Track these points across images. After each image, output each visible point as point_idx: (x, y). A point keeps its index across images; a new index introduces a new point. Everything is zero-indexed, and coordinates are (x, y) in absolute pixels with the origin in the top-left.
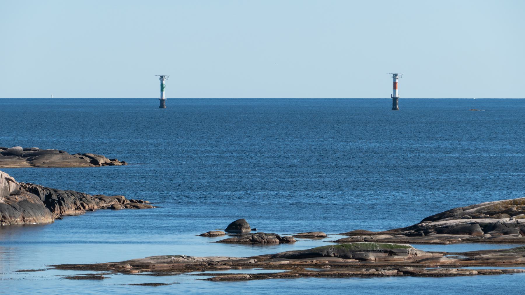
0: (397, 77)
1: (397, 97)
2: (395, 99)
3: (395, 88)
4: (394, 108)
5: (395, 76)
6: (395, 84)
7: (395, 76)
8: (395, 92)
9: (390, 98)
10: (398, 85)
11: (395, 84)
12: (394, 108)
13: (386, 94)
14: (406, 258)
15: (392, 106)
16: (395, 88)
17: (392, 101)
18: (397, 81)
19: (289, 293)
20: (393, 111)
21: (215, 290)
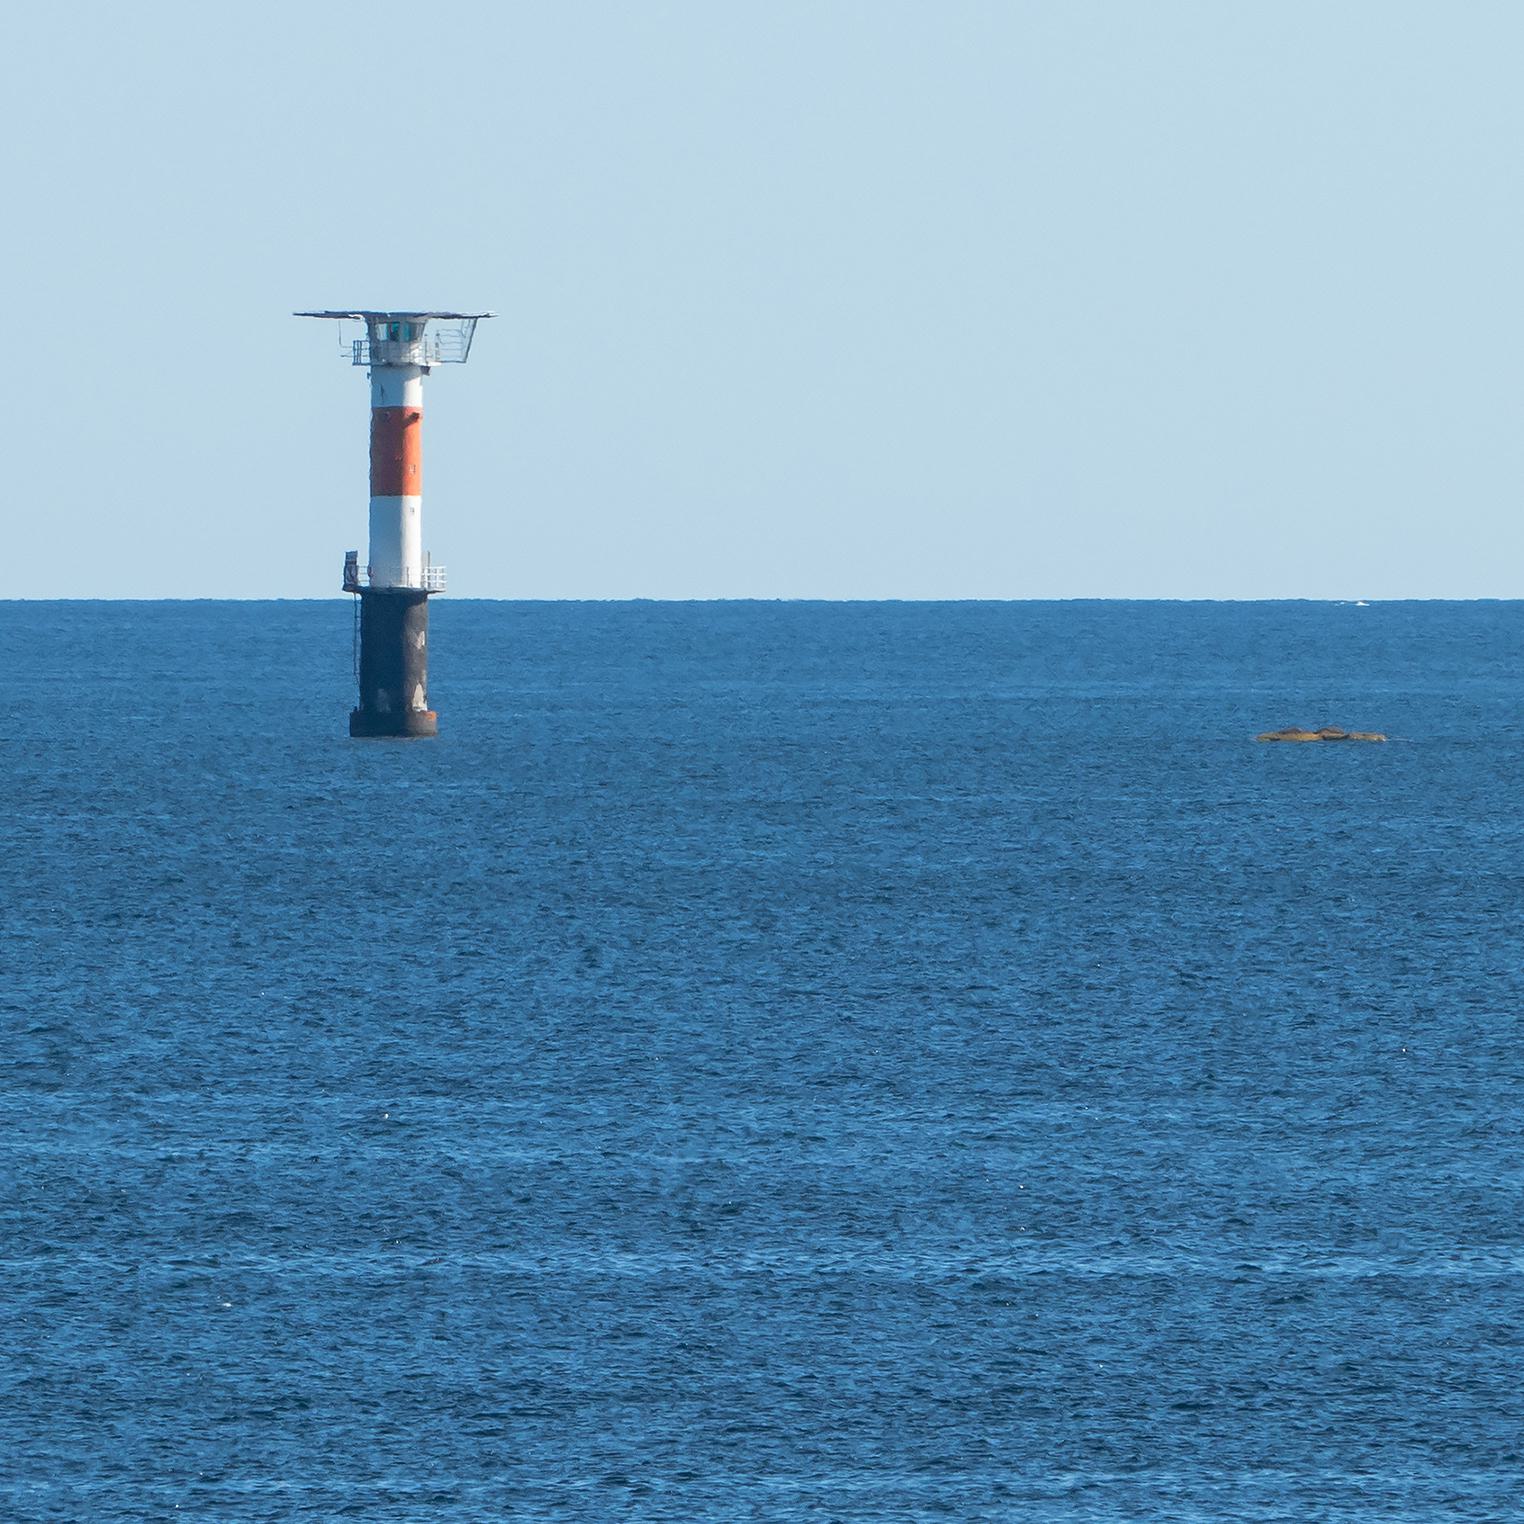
0: (417, 354)
1: (414, 580)
2: (386, 614)
3: (389, 473)
4: (381, 712)
5: (390, 340)
6: (391, 431)
7: (390, 340)
8: (387, 530)
9: (331, 588)
10: (424, 446)
11: (391, 431)
12: (381, 712)
13: (283, 543)
14: (991, 1127)
15: (355, 700)
16: (389, 473)
17: (348, 635)
18: (415, 394)
19: (904, 1519)
20: (375, 749)
21: (1394, 1516)
